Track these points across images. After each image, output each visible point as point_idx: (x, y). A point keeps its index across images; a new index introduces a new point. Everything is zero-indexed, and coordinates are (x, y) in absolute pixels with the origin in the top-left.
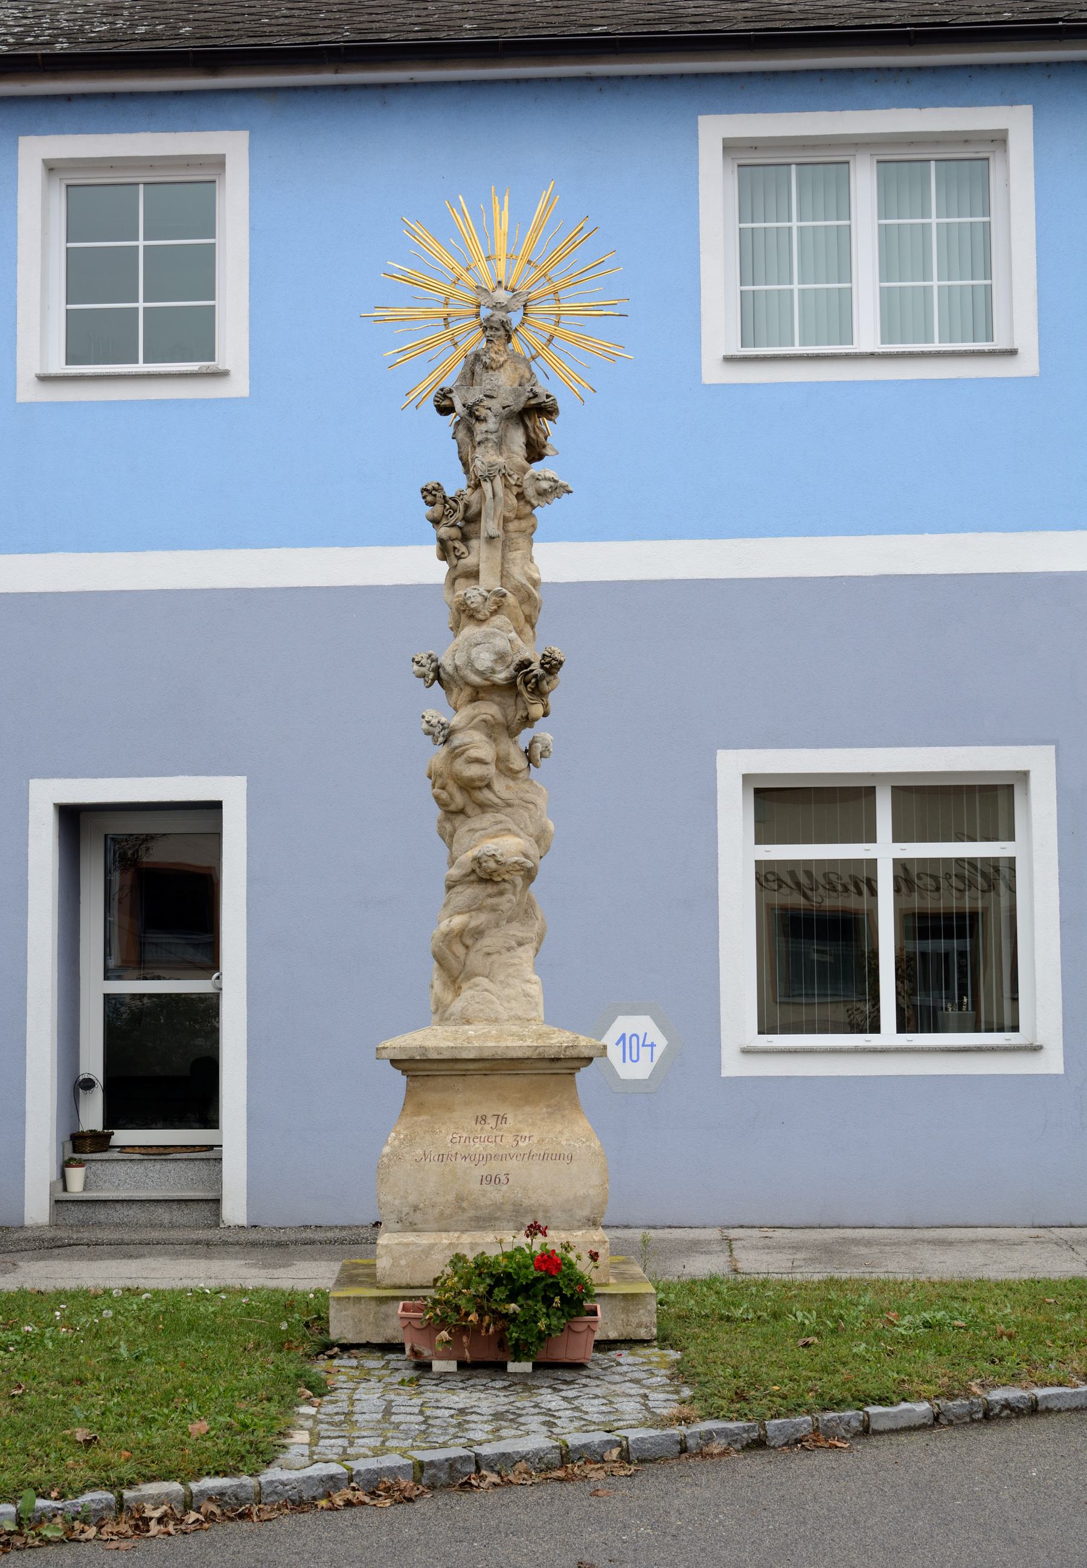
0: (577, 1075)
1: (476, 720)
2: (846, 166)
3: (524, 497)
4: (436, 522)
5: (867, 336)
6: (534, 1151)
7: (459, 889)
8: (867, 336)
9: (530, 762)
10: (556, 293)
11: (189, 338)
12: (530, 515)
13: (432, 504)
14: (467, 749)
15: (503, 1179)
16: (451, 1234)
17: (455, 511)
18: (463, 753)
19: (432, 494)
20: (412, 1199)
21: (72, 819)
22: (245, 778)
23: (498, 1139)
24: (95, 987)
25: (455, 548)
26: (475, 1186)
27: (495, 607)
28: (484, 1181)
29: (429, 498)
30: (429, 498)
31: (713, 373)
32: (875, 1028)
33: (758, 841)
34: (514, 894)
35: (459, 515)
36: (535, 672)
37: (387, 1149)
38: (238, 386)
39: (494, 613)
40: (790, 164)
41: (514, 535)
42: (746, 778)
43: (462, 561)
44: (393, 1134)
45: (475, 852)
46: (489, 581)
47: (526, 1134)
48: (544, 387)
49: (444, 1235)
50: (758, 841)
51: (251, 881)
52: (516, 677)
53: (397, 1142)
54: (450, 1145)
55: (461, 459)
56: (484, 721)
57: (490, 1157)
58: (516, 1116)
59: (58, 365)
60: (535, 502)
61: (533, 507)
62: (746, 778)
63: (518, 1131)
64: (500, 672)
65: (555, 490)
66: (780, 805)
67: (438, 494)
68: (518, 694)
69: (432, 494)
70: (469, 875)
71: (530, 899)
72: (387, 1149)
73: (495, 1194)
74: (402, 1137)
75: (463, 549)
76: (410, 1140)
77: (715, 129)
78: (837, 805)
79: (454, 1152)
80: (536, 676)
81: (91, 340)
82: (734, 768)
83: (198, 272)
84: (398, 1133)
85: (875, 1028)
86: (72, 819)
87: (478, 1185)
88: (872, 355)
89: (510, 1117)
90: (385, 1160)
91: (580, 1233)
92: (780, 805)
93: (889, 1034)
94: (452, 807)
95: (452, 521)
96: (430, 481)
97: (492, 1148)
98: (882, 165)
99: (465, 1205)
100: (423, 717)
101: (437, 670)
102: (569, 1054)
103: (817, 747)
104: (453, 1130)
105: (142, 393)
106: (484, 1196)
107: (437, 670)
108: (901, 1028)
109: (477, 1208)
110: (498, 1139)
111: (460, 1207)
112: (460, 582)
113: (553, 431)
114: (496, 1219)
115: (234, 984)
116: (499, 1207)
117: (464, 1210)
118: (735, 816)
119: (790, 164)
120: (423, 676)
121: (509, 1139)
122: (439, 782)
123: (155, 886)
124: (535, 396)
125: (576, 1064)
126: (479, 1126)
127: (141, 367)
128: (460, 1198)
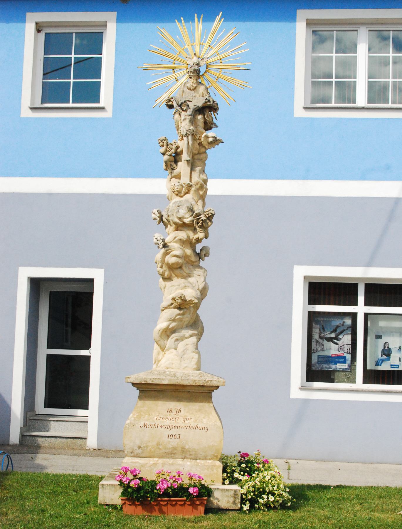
0: (212, 393)
2: (356, 32)
3: (202, 145)
5: (361, 99)
7: (166, 310)
8: (361, 99)
9: (200, 258)
10: (220, 59)
11: (90, 94)
12: (205, 152)
15: (178, 437)
16: (155, 459)
17: (172, 149)
18: (170, 253)
19: (164, 142)
20: (138, 443)
21: (36, 284)
22: (103, 270)
23: (177, 419)
24: (43, 352)
25: (171, 165)
31: (299, 112)
32: (354, 382)
33: (310, 303)
34: (189, 314)
35: (173, 151)
39: (186, 193)
40: (333, 31)
41: (197, 161)
42: (305, 278)
44: (131, 415)
48: (213, 98)
49: (151, 459)
50: (310, 303)
51: (104, 311)
52: (193, 221)
53: (133, 419)
54: (155, 421)
56: (180, 239)
59: (38, 104)
60: (207, 147)
61: (206, 149)
62: (305, 278)
63: (185, 416)
64: (187, 218)
65: (216, 141)
67: (165, 142)
68: (195, 229)
69: (164, 142)
71: (197, 315)
72: (128, 422)
73: (174, 443)
75: (175, 166)
76: (139, 418)
77: (304, 15)
79: (157, 424)
81: (52, 94)
83: (93, 68)
84: (134, 415)
85: (354, 382)
86: (36, 284)
88: (363, 108)
89: (182, 410)
90: (127, 426)
91: (210, 461)
92: (319, 291)
97: (173, 423)
98: (371, 32)
99: (161, 447)
101: (161, 217)
102: (208, 384)
103: (335, 266)
104: (157, 415)
105: (70, 116)
107: (161, 217)
108: (364, 382)
109: (166, 448)
110: (177, 419)
111: (159, 448)
112: (173, 179)
113: (219, 118)
114: (174, 454)
115: (95, 353)
116: (175, 449)
117: (160, 449)
119: (333, 31)
120: (155, 219)
121: (181, 420)
124: (209, 101)
125: (212, 389)
126: (169, 413)
128: (158, 444)
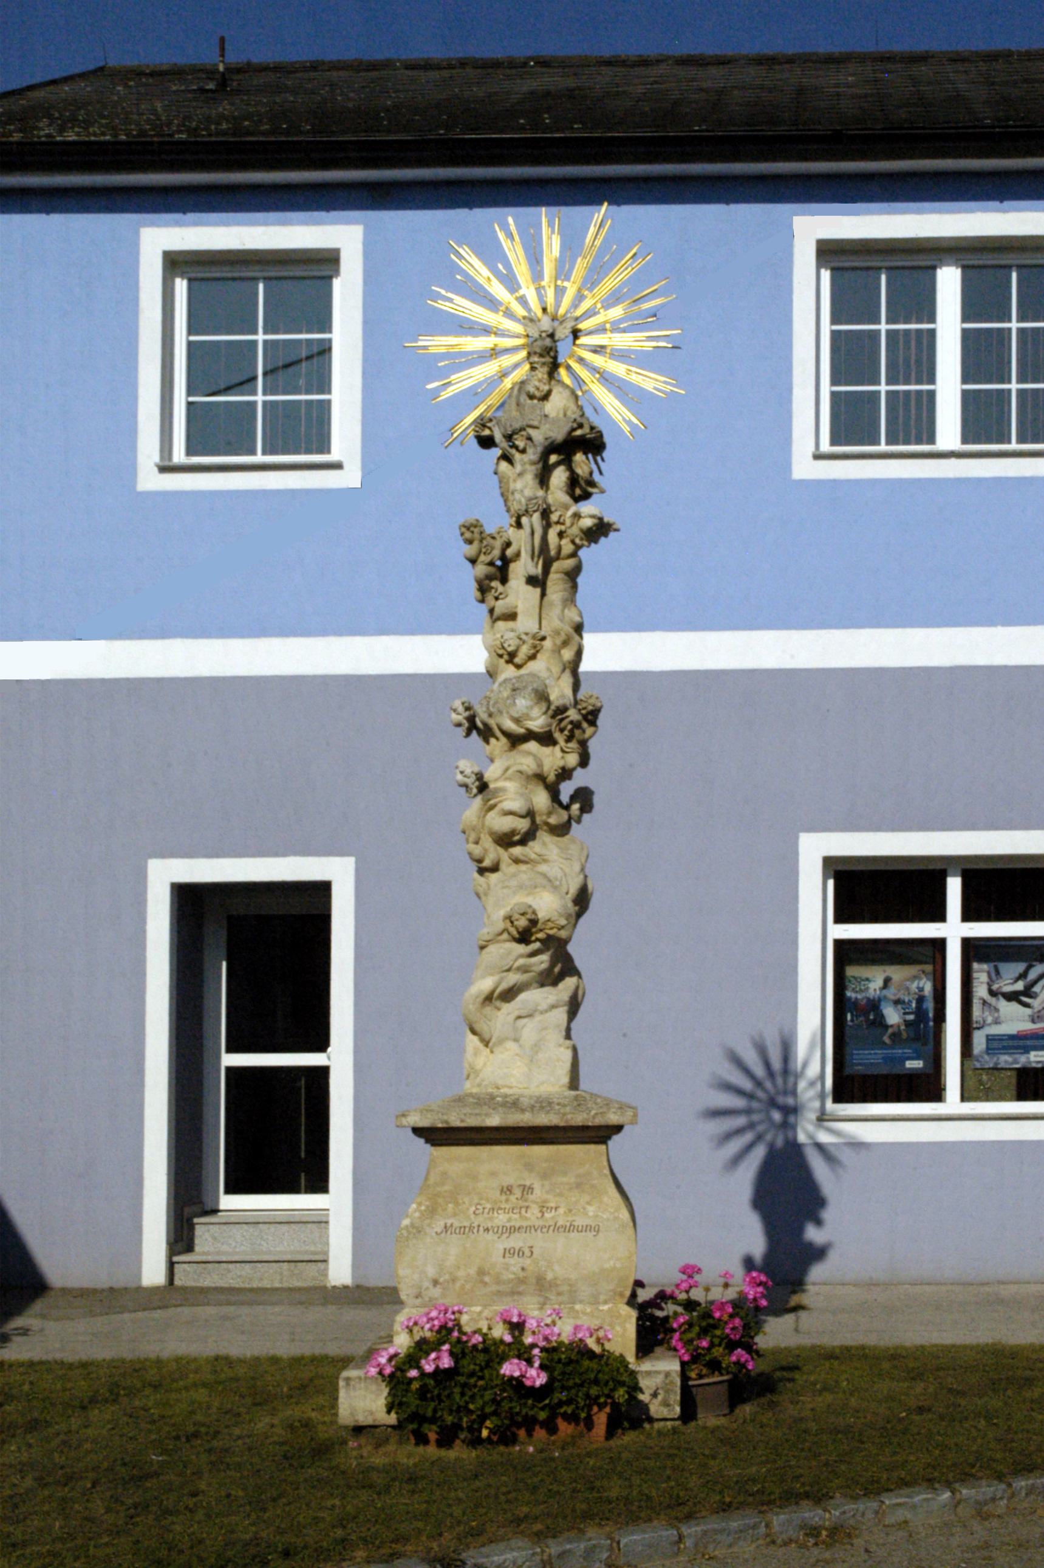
1: (510, 771)
4: (473, 561)
6: (560, 1223)
11: (303, 432)
13: (470, 542)
14: (500, 802)
15: (527, 1252)
19: (472, 531)
26: (497, 1258)
27: (532, 651)
28: (507, 1255)
29: (468, 535)
30: (468, 535)
36: (571, 718)
37: (406, 1222)
38: (350, 477)
43: (500, 602)
45: (502, 913)
46: (526, 623)
47: (553, 1205)
54: (472, 1216)
55: (502, 495)
57: (512, 1230)
58: (543, 1186)
66: (860, 888)
69: (472, 531)
70: (501, 934)
74: (423, 1208)
78: (908, 888)
79: (475, 1225)
80: (571, 722)
82: (815, 848)
84: (420, 1204)
87: (501, 1259)
92: (860, 888)
93: (952, 1101)
94: (487, 863)
95: (488, 559)
96: (470, 518)
97: (516, 1220)
99: (487, 1279)
100: (457, 767)
101: (471, 719)
104: (476, 1201)
106: (507, 1269)
118: (814, 894)
119: (880, 268)
121: (535, 1211)
122: (473, 836)
123: (259, 957)
126: (504, 1197)
127: (259, 458)
128: (481, 1272)
